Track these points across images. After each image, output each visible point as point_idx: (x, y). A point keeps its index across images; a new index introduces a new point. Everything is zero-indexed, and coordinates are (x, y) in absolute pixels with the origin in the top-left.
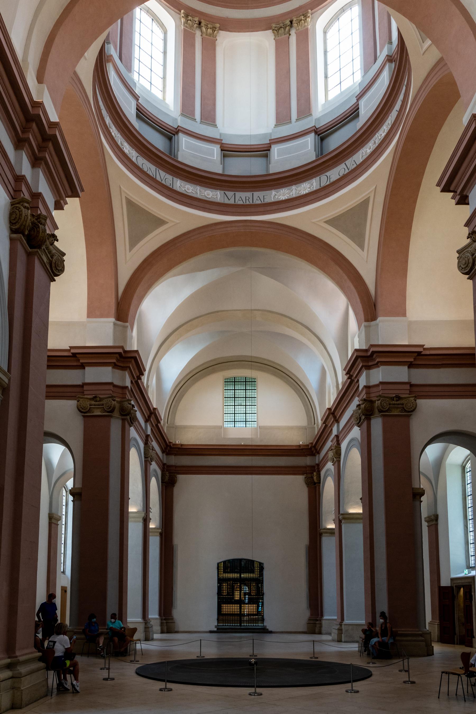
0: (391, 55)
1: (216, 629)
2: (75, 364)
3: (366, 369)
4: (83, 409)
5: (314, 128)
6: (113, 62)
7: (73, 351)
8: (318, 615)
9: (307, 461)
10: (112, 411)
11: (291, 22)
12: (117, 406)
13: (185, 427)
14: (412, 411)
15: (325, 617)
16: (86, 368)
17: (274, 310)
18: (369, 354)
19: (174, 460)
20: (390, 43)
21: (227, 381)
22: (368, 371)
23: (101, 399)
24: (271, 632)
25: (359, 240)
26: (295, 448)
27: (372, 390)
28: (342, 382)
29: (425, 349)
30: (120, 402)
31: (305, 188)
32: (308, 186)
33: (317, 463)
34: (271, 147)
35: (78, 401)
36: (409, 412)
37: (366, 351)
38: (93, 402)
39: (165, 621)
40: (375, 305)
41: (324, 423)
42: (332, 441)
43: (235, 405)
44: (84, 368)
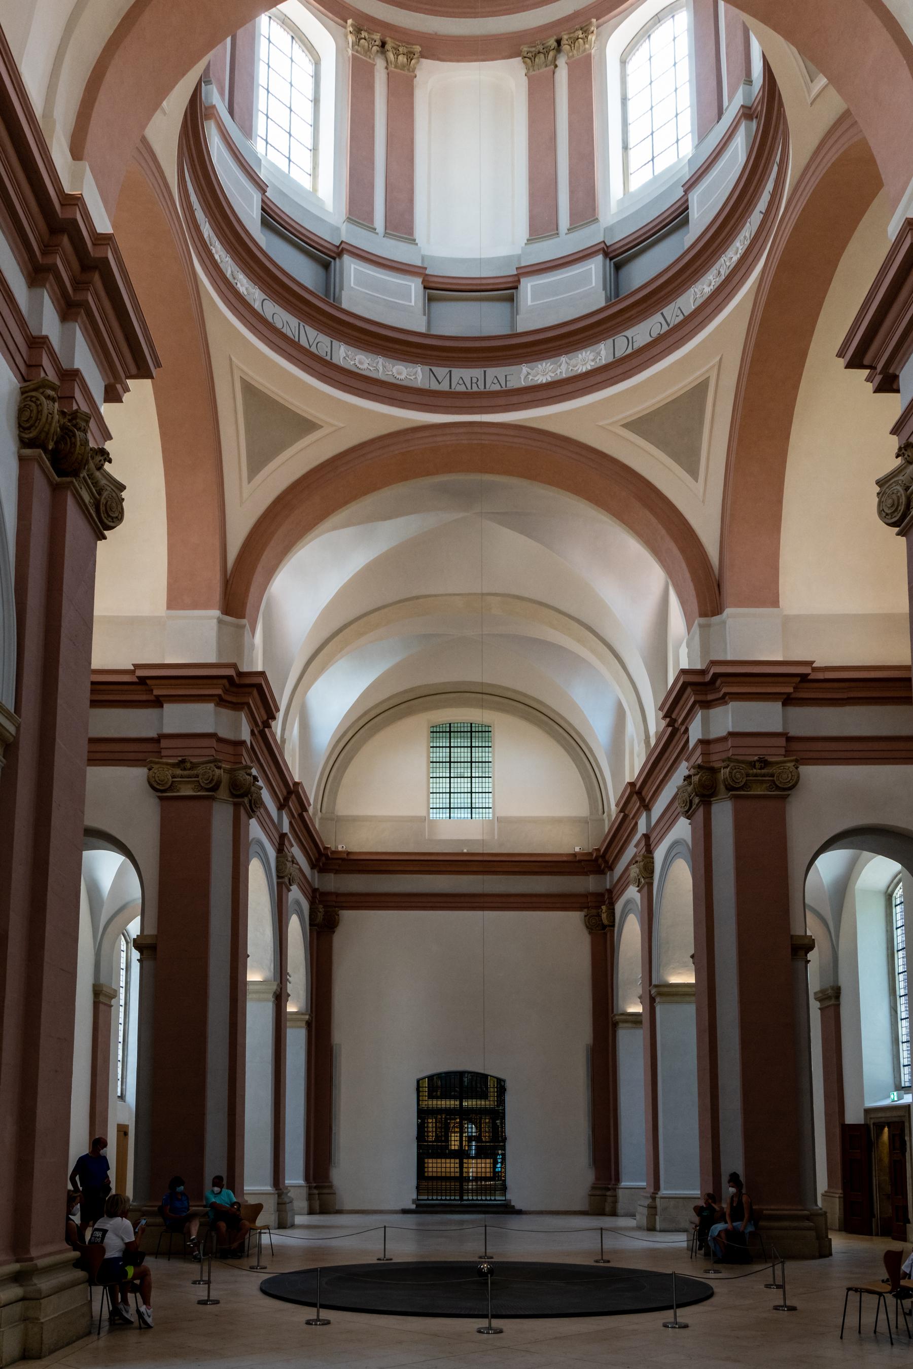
0: (750, 105)
1: (414, 1207)
2: (144, 697)
3: (702, 707)
4: (159, 784)
5: (603, 245)
6: (216, 119)
7: (140, 673)
8: (611, 1179)
9: (589, 884)
10: (215, 788)
11: (559, 42)
12: (225, 778)
13: (355, 819)
14: (790, 789)
15: (623, 1184)
16: (165, 705)
17: (526, 594)
18: (708, 678)
19: (333, 883)
20: (749, 82)
21: (436, 731)
22: (705, 711)
23: (194, 766)
24: (520, 1212)
25: (689, 459)
26: (565, 859)
27: (714, 748)
28: (656, 732)
29: (815, 669)
30: (230, 772)
31: (585, 360)
32: (591, 357)
33: (608, 887)
34: (519, 281)
35: (150, 770)
36: (784, 789)
37: (702, 672)
38: (179, 772)
39: (316, 1192)
40: (719, 586)
41: (621, 811)
42: (636, 846)
43: (450, 777)
44: (162, 706)
